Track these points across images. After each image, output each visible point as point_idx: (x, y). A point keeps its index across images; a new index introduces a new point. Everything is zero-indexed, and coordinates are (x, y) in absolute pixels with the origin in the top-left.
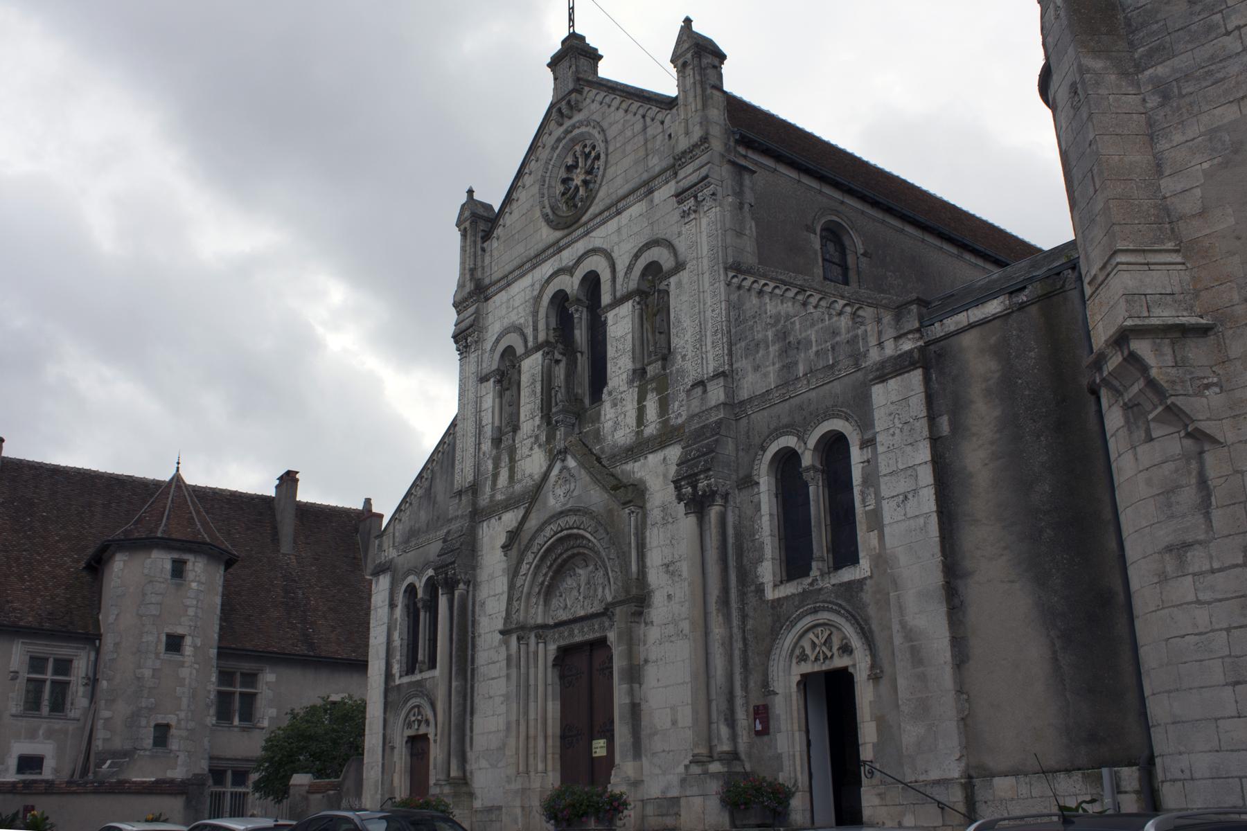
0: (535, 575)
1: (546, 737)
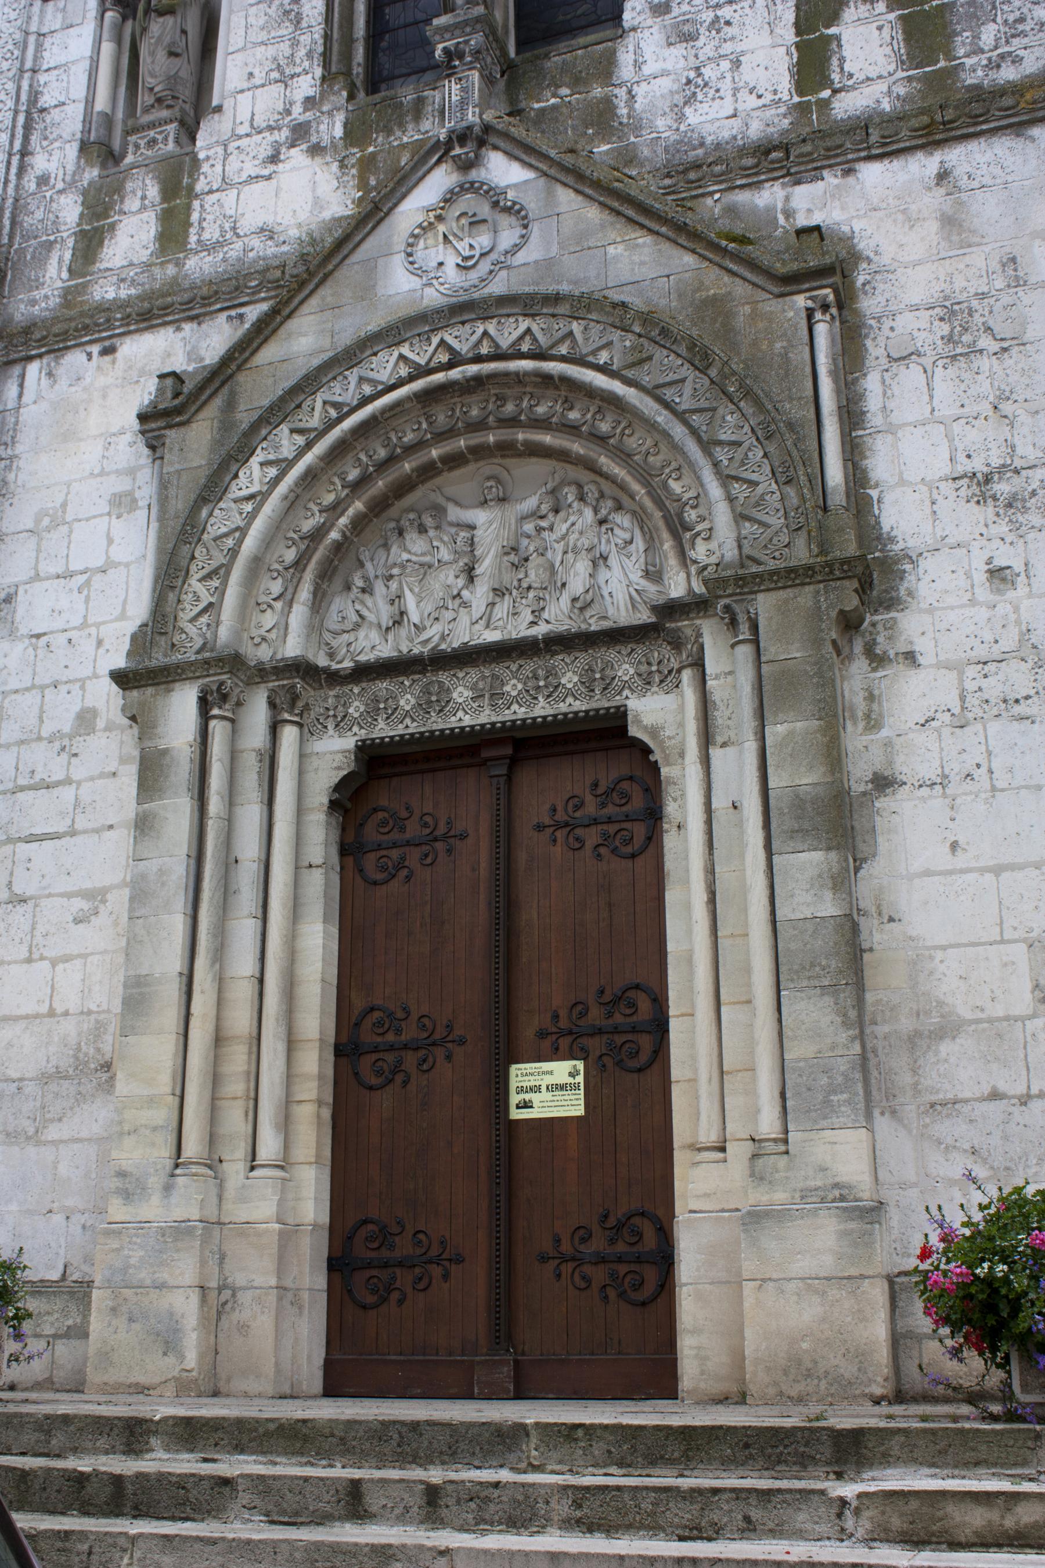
0: (293, 502)
1: (291, 1044)
